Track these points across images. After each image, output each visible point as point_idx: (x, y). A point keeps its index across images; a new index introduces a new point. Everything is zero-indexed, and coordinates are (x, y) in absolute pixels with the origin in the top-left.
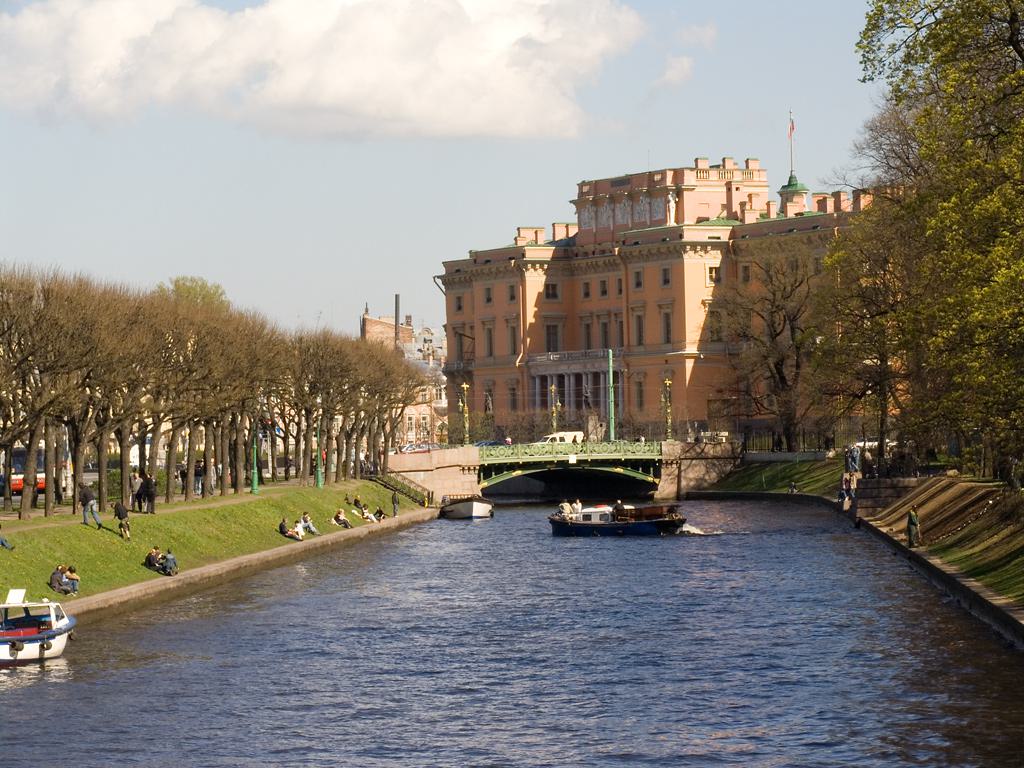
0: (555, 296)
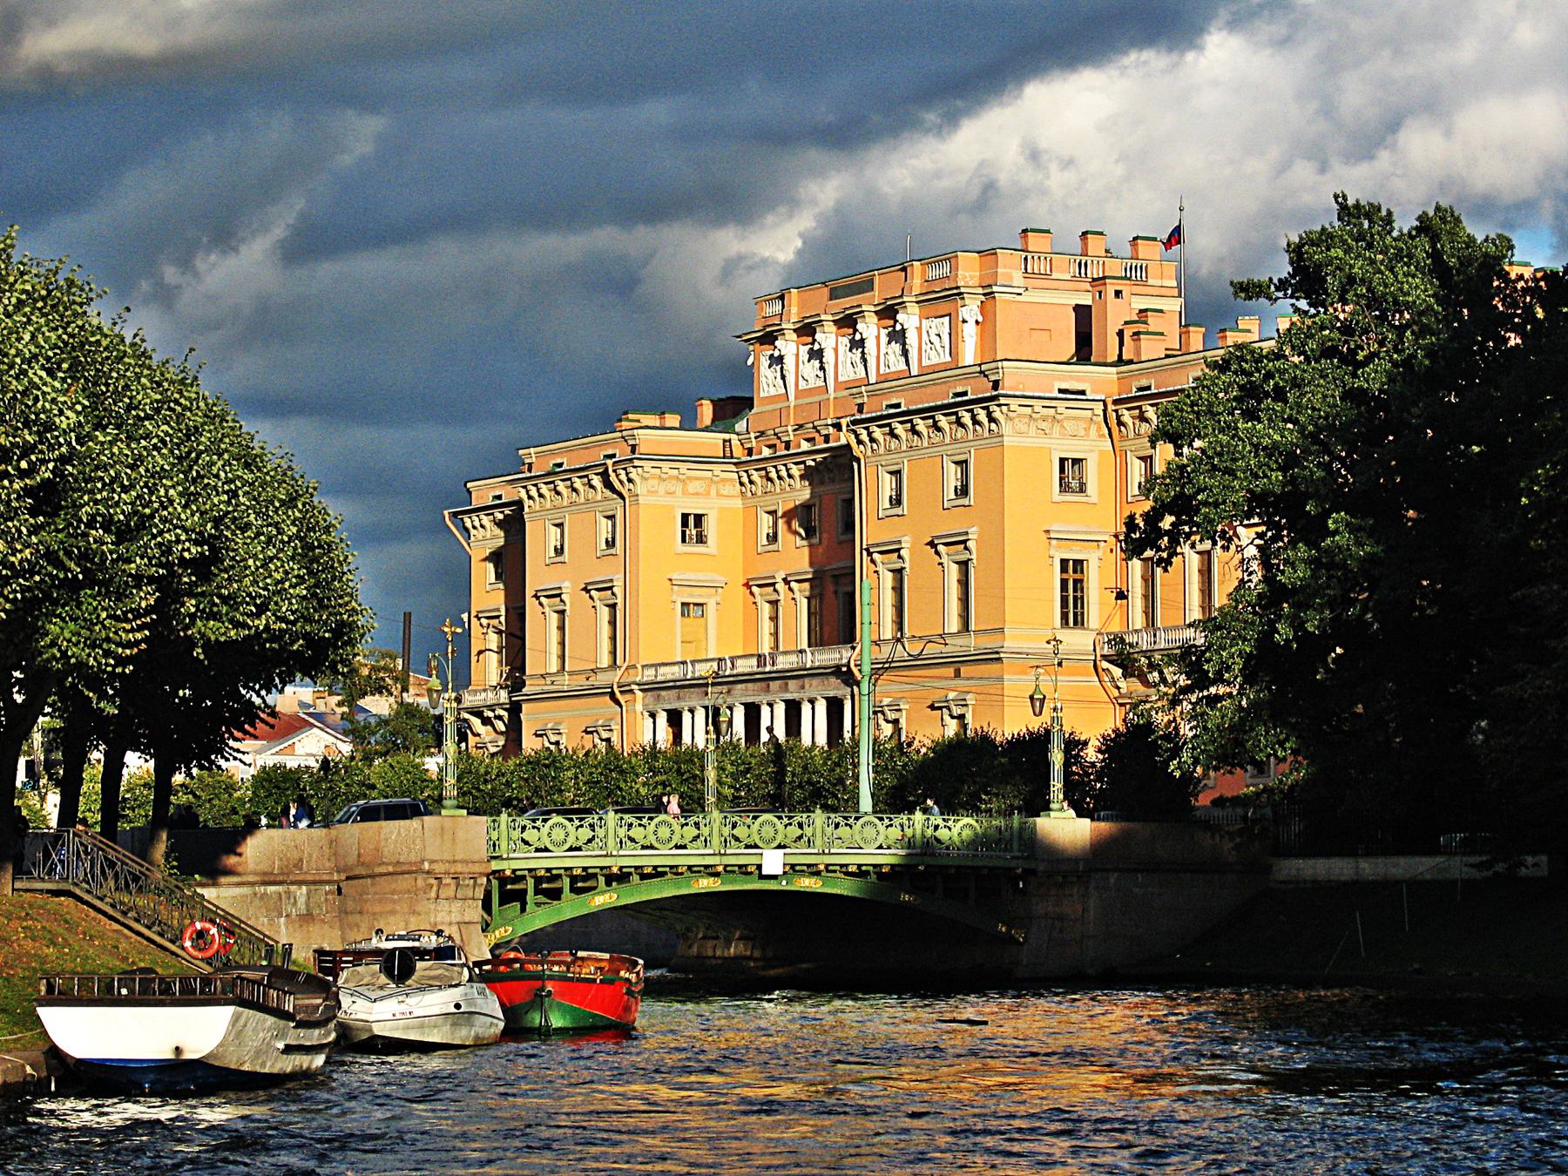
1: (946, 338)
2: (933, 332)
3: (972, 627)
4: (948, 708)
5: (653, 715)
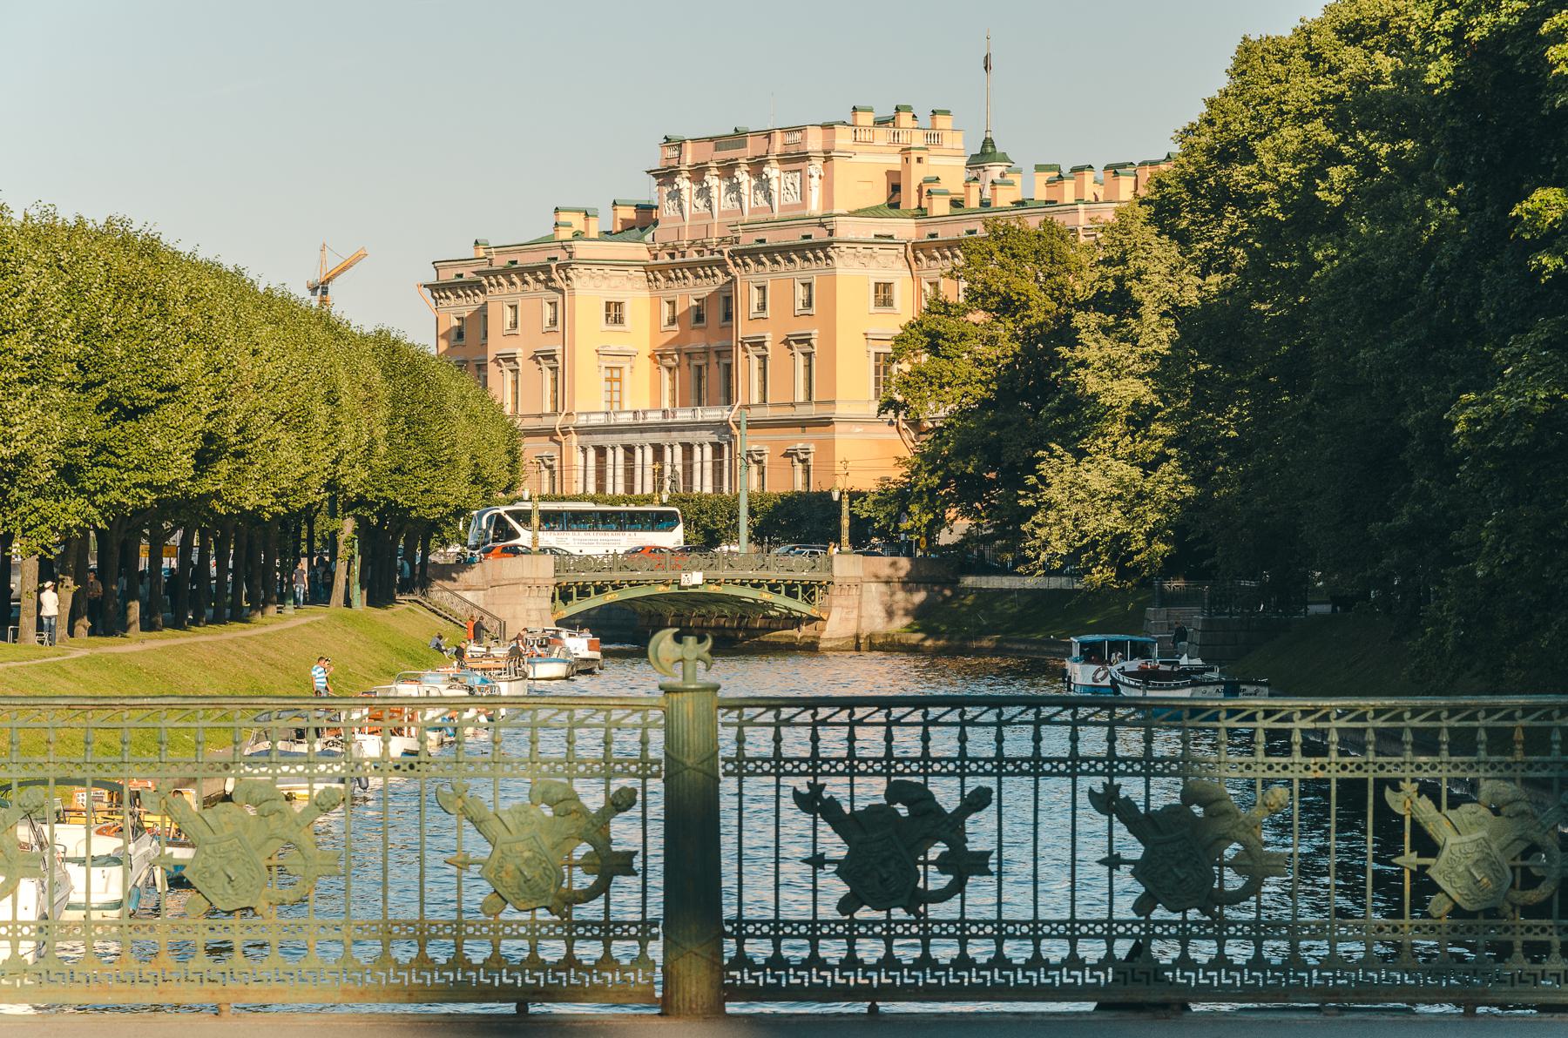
0: (618, 320)
1: (798, 186)
2: (789, 180)
3: (814, 399)
4: (797, 454)
5: (584, 450)
